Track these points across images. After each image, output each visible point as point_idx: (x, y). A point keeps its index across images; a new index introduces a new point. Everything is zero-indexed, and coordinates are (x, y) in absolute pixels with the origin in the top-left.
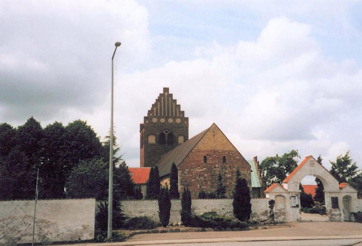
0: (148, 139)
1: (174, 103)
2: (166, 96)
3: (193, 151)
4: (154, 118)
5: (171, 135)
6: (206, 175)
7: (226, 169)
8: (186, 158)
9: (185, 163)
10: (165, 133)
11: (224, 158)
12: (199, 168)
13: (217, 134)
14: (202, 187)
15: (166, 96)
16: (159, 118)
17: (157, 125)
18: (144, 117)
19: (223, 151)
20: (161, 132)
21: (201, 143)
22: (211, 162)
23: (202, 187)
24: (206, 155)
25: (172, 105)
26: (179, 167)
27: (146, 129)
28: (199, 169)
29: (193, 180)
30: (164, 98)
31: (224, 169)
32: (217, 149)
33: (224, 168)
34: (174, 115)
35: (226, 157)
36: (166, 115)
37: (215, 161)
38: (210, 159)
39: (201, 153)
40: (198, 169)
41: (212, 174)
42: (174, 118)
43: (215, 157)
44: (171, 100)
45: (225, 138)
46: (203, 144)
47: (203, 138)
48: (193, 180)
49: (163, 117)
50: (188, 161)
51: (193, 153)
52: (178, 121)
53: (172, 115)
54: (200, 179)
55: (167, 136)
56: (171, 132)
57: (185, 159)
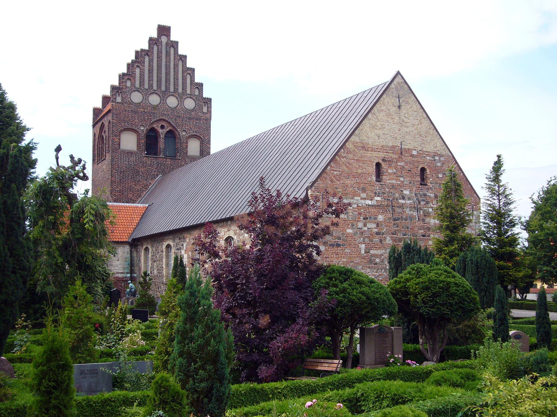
0: (120, 139)
1: (180, 63)
2: (164, 44)
3: (349, 145)
4: (135, 91)
5: (171, 134)
6: (381, 218)
7: (428, 203)
8: (332, 164)
9: (328, 178)
10: (160, 131)
11: (423, 170)
12: (364, 195)
13: (407, 103)
14: (372, 252)
15: (164, 44)
16: (147, 93)
17: (142, 110)
18: (148, 39)
19: (421, 154)
20: (151, 127)
21: (368, 125)
22: (394, 182)
23: (372, 252)
24: (380, 161)
25: (176, 66)
26: (313, 188)
27: (108, 120)
28: (364, 199)
29: (349, 231)
30: (158, 50)
31: (422, 203)
32: (406, 147)
33: (423, 200)
34: (180, 90)
35: (428, 171)
36: (163, 88)
37: (402, 179)
38: (390, 171)
39: (369, 154)
40: (362, 199)
41: (396, 216)
42: (181, 97)
43: (403, 168)
44: (175, 54)
45: (425, 116)
46: (374, 127)
47: (373, 111)
48: (349, 231)
49: (154, 93)
50: (335, 173)
51: (349, 152)
52: (189, 104)
53: (176, 89)
54: (366, 229)
55: (162, 136)
56: (174, 127)
57: (329, 167)
